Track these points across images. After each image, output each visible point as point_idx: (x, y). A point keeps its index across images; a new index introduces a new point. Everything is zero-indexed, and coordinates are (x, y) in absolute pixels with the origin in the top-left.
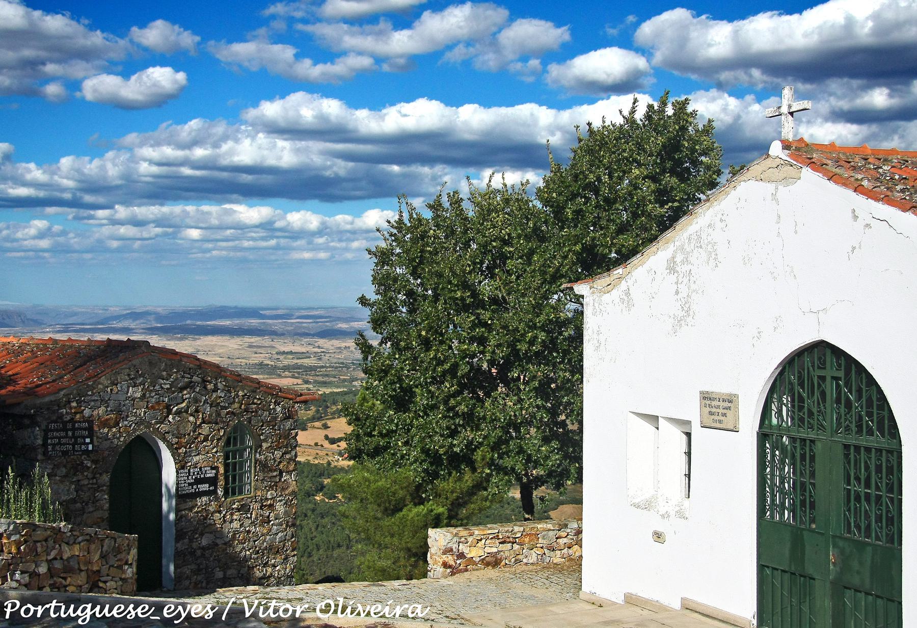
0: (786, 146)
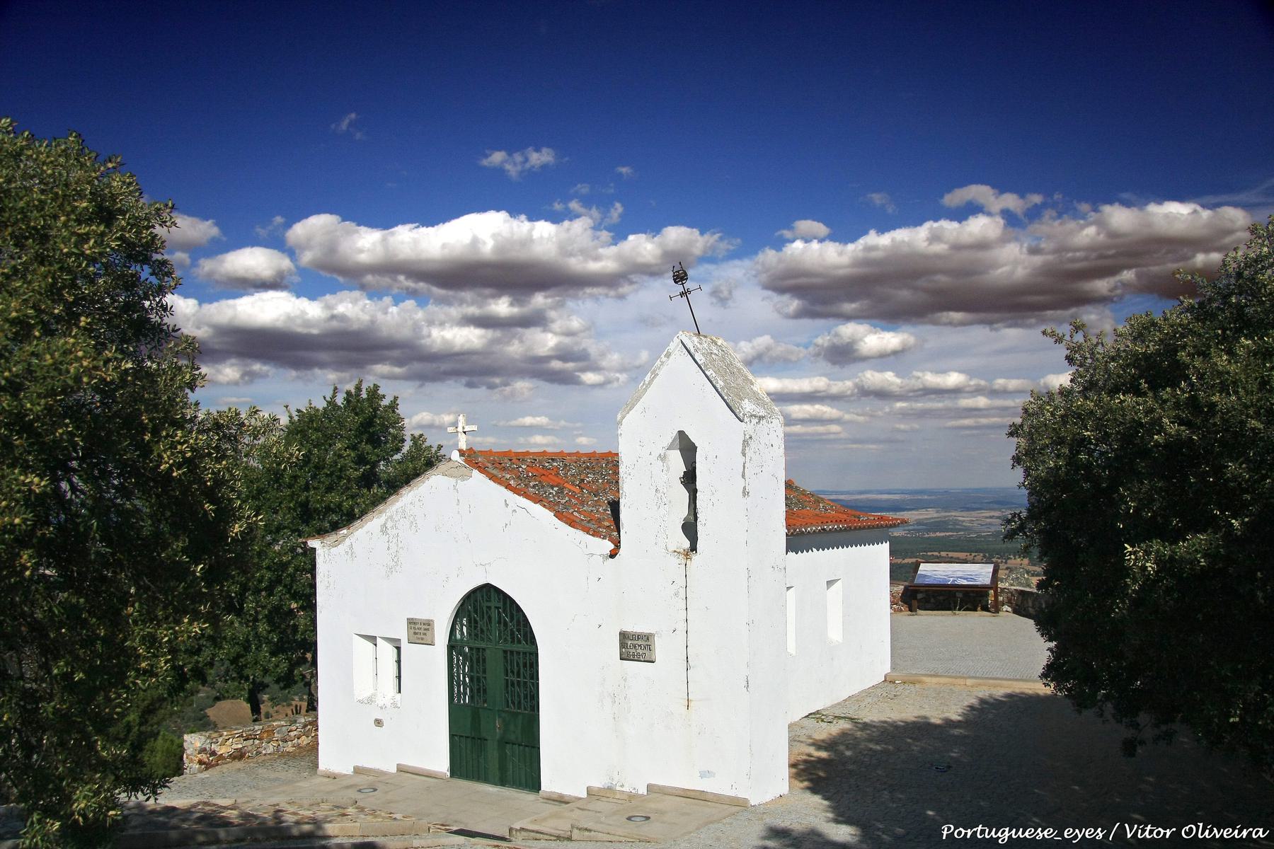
0: (462, 453)
